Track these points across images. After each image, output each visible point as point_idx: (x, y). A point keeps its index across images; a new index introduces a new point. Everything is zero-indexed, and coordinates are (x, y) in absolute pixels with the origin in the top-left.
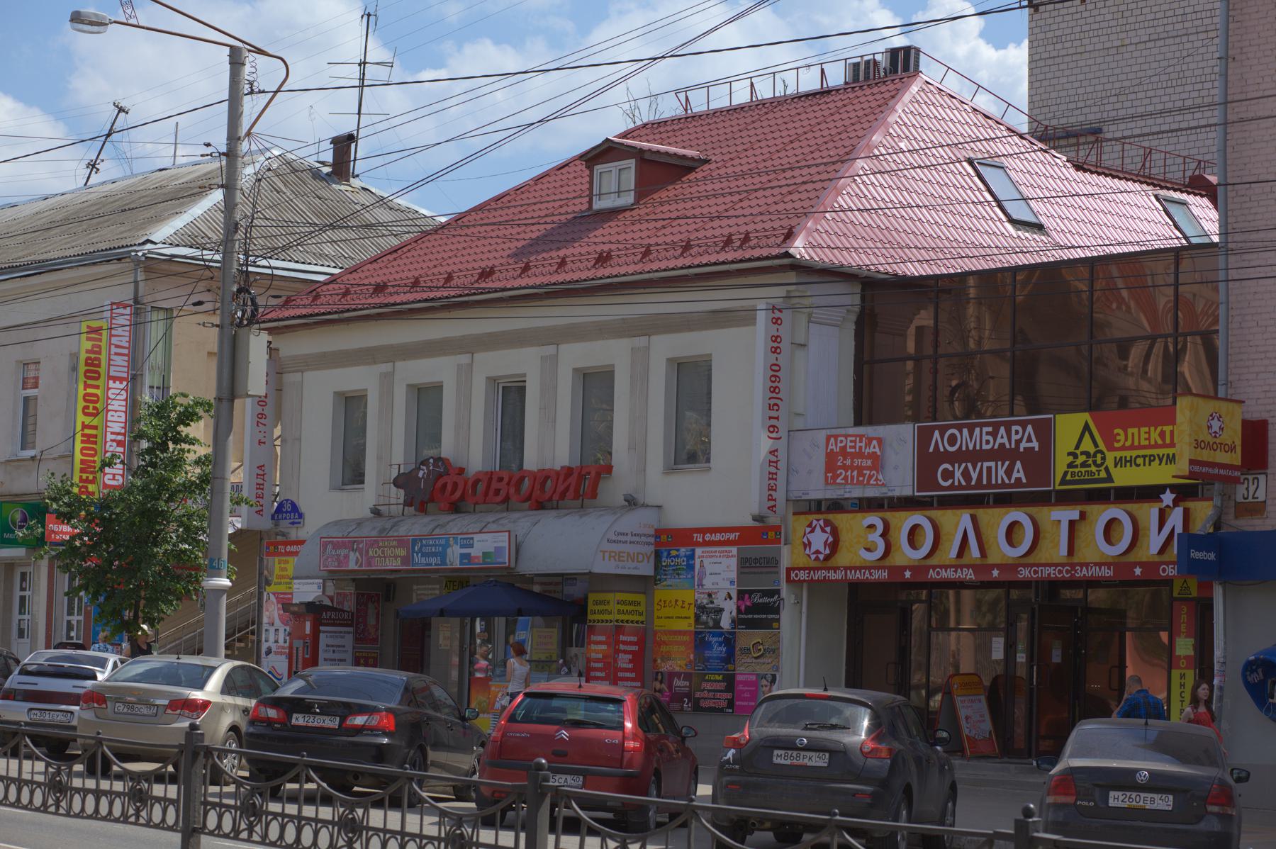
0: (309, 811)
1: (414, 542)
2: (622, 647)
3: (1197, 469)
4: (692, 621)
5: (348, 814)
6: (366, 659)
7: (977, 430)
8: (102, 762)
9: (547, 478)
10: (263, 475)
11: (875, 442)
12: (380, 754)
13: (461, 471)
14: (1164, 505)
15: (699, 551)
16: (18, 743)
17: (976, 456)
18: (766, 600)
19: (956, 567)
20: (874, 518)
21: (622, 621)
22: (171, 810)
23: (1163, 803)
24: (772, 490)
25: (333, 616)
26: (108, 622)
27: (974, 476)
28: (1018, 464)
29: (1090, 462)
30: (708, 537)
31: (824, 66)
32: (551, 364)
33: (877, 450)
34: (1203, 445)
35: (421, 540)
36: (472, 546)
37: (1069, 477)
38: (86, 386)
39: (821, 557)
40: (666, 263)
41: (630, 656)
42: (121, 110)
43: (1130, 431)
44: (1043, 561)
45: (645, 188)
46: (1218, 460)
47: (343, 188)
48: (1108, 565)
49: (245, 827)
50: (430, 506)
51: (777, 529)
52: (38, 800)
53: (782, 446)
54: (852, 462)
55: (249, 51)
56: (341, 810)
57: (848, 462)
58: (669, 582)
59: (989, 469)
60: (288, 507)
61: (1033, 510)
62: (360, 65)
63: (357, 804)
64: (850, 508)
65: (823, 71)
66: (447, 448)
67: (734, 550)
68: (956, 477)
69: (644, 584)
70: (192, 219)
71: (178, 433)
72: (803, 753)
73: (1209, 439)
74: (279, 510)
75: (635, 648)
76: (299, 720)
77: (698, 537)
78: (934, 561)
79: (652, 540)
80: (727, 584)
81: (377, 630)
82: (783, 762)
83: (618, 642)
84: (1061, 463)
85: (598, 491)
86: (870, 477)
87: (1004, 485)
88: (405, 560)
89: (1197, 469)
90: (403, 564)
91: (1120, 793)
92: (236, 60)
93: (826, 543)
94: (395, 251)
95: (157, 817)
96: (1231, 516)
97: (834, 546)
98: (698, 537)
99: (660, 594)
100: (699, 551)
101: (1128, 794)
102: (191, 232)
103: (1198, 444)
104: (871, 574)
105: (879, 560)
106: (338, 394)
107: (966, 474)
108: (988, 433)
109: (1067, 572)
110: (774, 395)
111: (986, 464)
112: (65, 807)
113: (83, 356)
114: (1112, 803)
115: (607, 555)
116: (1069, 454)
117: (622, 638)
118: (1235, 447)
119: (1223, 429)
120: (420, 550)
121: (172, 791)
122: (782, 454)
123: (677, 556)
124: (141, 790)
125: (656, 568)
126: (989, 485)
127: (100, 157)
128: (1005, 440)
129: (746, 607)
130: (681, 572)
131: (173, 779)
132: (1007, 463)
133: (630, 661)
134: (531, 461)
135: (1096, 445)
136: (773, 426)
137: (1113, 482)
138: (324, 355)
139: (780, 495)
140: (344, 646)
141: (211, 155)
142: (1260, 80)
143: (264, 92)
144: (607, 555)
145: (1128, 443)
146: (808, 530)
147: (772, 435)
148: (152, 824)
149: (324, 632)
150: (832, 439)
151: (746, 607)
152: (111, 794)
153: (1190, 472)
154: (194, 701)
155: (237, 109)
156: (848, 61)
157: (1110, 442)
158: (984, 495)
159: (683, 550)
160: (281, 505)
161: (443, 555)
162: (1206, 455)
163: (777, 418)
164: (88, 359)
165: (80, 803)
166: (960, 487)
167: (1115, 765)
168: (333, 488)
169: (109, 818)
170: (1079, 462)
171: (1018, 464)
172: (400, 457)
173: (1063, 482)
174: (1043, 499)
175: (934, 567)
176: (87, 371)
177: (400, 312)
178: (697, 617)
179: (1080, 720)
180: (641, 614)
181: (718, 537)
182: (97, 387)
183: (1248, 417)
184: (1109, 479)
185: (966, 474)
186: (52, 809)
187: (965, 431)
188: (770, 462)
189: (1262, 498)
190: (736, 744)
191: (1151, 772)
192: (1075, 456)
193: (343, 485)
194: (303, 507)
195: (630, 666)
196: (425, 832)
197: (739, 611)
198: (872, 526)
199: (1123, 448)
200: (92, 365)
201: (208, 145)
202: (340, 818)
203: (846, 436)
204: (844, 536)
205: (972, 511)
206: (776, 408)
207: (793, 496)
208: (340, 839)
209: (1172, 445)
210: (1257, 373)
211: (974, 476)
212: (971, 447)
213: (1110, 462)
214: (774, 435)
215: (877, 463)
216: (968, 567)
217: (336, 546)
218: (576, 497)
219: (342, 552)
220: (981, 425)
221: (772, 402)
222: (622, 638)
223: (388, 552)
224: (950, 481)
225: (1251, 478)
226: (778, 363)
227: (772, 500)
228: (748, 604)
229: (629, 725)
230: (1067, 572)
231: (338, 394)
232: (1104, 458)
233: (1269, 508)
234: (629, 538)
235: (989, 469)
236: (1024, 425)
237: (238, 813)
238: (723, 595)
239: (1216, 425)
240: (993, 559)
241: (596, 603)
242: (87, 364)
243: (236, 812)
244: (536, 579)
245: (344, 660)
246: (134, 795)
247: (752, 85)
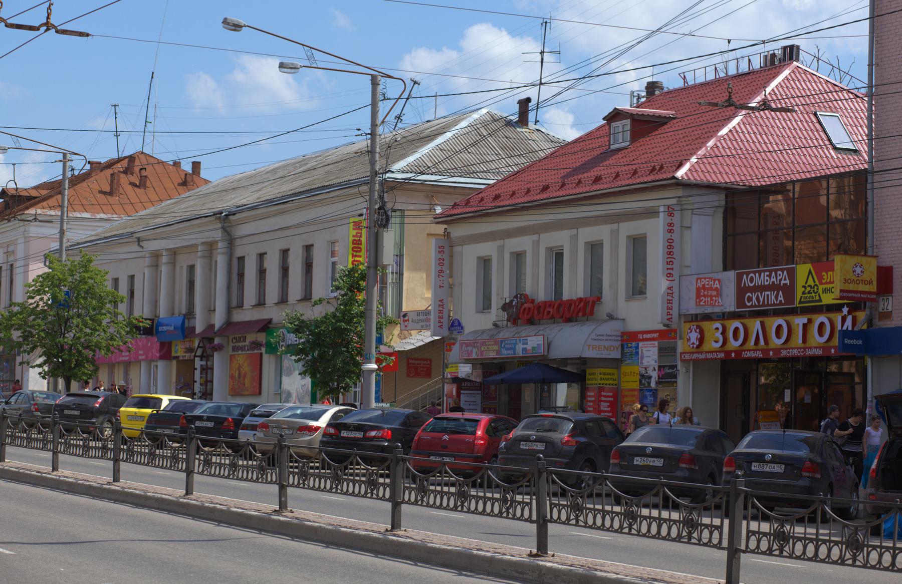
0: (446, 489)
1: (502, 342)
2: (603, 399)
3: (845, 294)
4: (638, 383)
5: (780, 529)
6: (490, 409)
7: (762, 274)
8: (822, 513)
9: (571, 305)
10: (672, 293)
11: (717, 282)
12: (383, 449)
13: (533, 301)
14: (843, 314)
15: (641, 344)
16: (483, 474)
17: (761, 288)
18: (670, 371)
19: (754, 350)
20: (718, 325)
21: (603, 384)
22: (388, 490)
23: (658, 462)
24: (670, 309)
25: (469, 385)
26: (321, 389)
27: (761, 299)
28: (781, 293)
29: (812, 291)
30: (645, 336)
31: (750, 57)
32: (615, 234)
33: (718, 286)
34: (849, 281)
35: (505, 341)
36: (527, 344)
37: (802, 300)
38: (353, 256)
39: (695, 346)
40: (625, 182)
41: (609, 404)
42: (115, 106)
43: (829, 273)
44: (793, 346)
45: (636, 135)
46: (860, 289)
47: (524, 130)
48: (820, 348)
49: (686, 534)
50: (519, 321)
51: (675, 331)
52: (616, 525)
53: (675, 284)
54: (708, 293)
55: (382, 76)
56: (776, 526)
57: (706, 293)
58: (627, 362)
59: (768, 295)
60: (456, 324)
61: (788, 318)
62: (541, 53)
63: (694, 508)
64: (716, 318)
65: (749, 60)
66: (528, 289)
67: (656, 343)
68: (753, 300)
69: (616, 363)
70: (420, 156)
71: (359, 285)
72: (534, 443)
73: (855, 279)
74: (452, 325)
75: (612, 399)
76: (344, 434)
77: (640, 336)
78: (745, 347)
79: (619, 338)
80: (653, 363)
81: (496, 392)
82: (525, 448)
83: (600, 396)
84: (799, 291)
85: (595, 311)
86: (716, 301)
87: (774, 305)
88: (498, 352)
89: (845, 294)
90: (497, 354)
91: (758, 464)
92: (374, 83)
93: (697, 338)
94: (516, 174)
95: (644, 530)
96: (877, 320)
97: (701, 340)
98: (640, 336)
99: (625, 369)
100: (641, 344)
101: (643, 458)
102: (418, 164)
103: (846, 281)
104: (717, 355)
105: (783, 344)
106: (479, 258)
107: (758, 298)
108: (767, 276)
109: (802, 352)
110: (670, 256)
111: (767, 293)
112: (697, 537)
113: (351, 238)
114: (635, 463)
115: (591, 347)
116: (803, 287)
117: (603, 393)
118: (872, 282)
119: (863, 272)
120: (504, 346)
121: (388, 481)
122: (676, 290)
123: (631, 347)
124: (633, 511)
125: (622, 354)
126: (768, 305)
127: (403, 112)
128: (775, 280)
129: (662, 375)
130: (633, 356)
131: (388, 476)
132: (776, 292)
133: (608, 407)
134: (566, 296)
135: (814, 282)
136: (670, 274)
137: (821, 302)
138: (471, 236)
139: (675, 312)
140: (476, 402)
141: (361, 135)
142: (889, 77)
143: (390, 99)
144: (591, 347)
145: (828, 280)
146: (689, 331)
147: (668, 279)
148: (641, 534)
149: (463, 394)
150: (699, 281)
151: (662, 375)
152: (493, 500)
153: (841, 296)
154: (311, 427)
155: (376, 109)
156: (762, 55)
157: (820, 278)
158: (767, 310)
159: (634, 344)
160: (453, 322)
161: (514, 349)
162: (851, 287)
163: (672, 269)
164: (354, 240)
165: (446, 501)
166: (755, 306)
167: (640, 445)
168: (477, 312)
169: (668, 538)
170: (807, 291)
171: (781, 293)
172: (507, 295)
173: (800, 302)
174: (793, 312)
175: (745, 351)
176: (353, 248)
177: (459, 219)
178: (640, 381)
179: (753, 430)
180: (615, 380)
181: (648, 336)
182: (360, 256)
183: (881, 265)
184: (820, 300)
185: (758, 298)
186: (573, 522)
187: (757, 274)
188: (668, 293)
189: (890, 310)
190: (506, 440)
191: (653, 448)
192: (806, 288)
193: (484, 310)
194: (464, 323)
195: (609, 409)
196: (761, 530)
197: (659, 378)
198: (717, 329)
199: (826, 283)
200: (356, 244)
201: (359, 130)
202: (684, 518)
203: (705, 278)
204: (706, 334)
205: (761, 319)
206: (671, 263)
207: (683, 312)
208: (775, 545)
209: (833, 283)
210: (888, 240)
211: (761, 299)
212: (760, 284)
213: (820, 291)
214: (670, 279)
215: (719, 293)
216: (759, 350)
217: (467, 345)
218: (584, 315)
219: (469, 348)
220: (764, 271)
221: (669, 260)
222: (603, 393)
223: (490, 348)
224: (751, 303)
225: (885, 298)
226: (672, 238)
227: (670, 315)
228: (663, 373)
229: (479, 433)
230: (802, 352)
231: (479, 258)
232: (818, 289)
233: (894, 315)
234: (604, 338)
235: (768, 295)
236: (782, 270)
237: (681, 525)
238: (651, 368)
239: (858, 270)
240: (771, 346)
241: (590, 374)
242: (353, 244)
243: (680, 525)
244: (569, 361)
245: (476, 410)
246: (461, 494)
247: (716, 69)
